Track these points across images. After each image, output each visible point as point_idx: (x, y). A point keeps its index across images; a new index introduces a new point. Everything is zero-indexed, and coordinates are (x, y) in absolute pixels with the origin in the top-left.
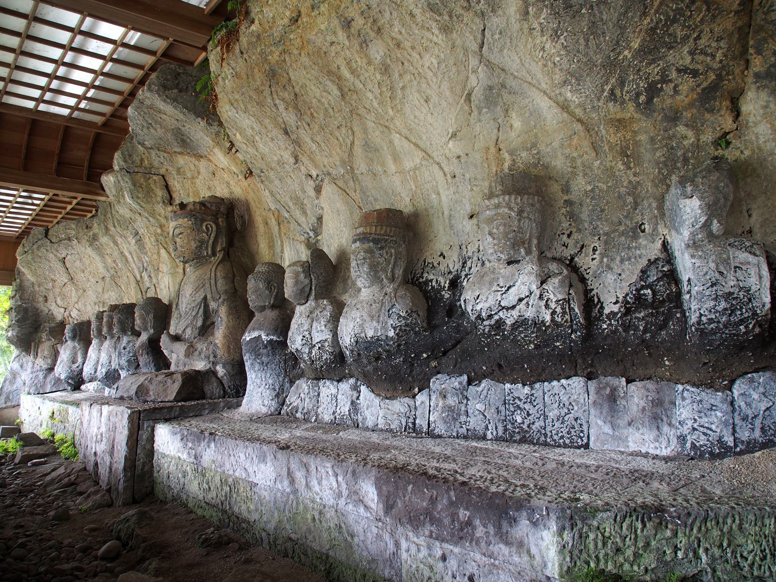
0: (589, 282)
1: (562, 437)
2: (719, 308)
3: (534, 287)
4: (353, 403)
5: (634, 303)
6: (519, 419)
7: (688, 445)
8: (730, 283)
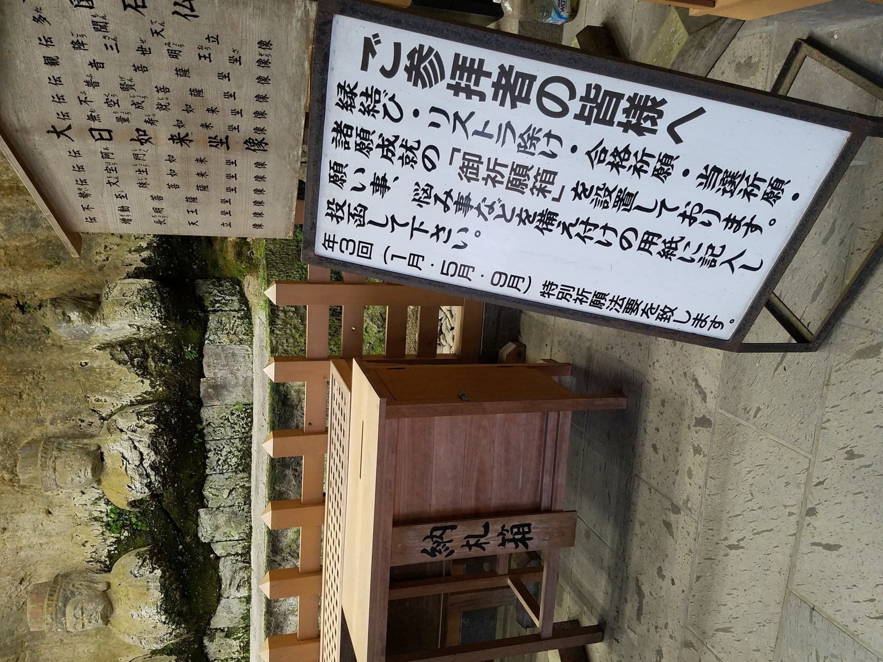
0: (124, 403)
1: (246, 424)
2: (151, 305)
3: (125, 437)
4: (228, 636)
5: (144, 371)
6: (234, 460)
7: (245, 337)
8: (136, 299)
